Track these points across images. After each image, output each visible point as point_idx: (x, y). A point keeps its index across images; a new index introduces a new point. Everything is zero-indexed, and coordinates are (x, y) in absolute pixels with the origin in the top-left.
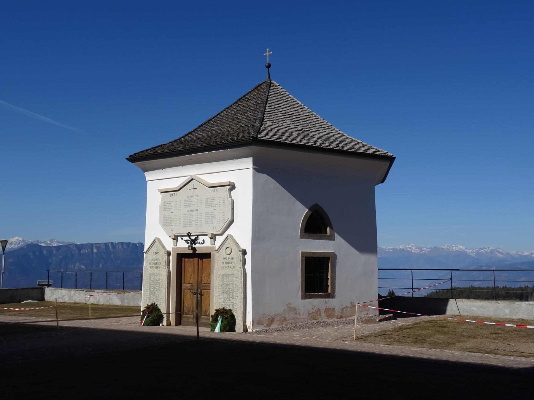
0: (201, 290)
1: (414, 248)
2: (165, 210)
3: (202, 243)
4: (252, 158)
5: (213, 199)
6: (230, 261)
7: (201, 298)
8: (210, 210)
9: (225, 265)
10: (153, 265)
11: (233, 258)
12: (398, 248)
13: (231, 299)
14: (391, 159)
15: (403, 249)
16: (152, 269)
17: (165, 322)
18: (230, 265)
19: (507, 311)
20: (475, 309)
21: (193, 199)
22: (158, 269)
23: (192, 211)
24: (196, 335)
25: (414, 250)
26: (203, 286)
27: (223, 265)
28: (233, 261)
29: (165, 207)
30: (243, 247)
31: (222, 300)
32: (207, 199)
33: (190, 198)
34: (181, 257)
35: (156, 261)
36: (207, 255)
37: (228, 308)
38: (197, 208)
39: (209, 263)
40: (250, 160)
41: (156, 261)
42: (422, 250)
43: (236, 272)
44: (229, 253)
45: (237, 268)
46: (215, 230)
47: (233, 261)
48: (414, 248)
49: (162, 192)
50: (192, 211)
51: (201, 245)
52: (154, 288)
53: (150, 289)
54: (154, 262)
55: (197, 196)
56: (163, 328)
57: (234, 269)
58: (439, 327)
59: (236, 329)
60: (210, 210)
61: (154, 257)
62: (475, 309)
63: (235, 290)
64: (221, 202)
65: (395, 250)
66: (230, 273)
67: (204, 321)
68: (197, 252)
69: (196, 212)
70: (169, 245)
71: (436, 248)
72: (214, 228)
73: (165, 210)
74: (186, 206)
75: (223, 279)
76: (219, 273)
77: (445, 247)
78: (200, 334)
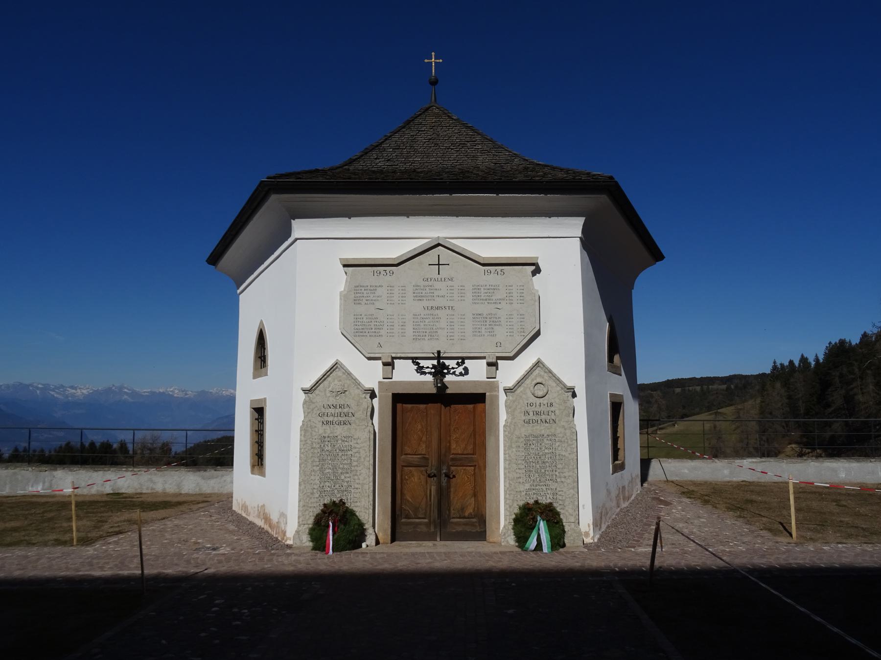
0: (448, 468)
1: (176, 391)
2: (357, 301)
3: (461, 374)
4: (579, 222)
5: (495, 288)
6: (543, 408)
7: (448, 482)
8: (485, 309)
9: (531, 416)
10: (330, 419)
11: (551, 405)
12: (157, 391)
13: (550, 483)
14: (658, 256)
15: (163, 393)
16: (327, 427)
17: (370, 540)
18: (543, 417)
19: (726, 472)
20: (686, 471)
21: (437, 285)
22: (346, 427)
23: (438, 308)
24: (648, 563)
25: (177, 394)
26: (453, 459)
27: (527, 418)
28: (552, 409)
29: (354, 297)
30: (368, 385)
31: (527, 486)
32: (476, 288)
33: (430, 283)
34: (401, 400)
35: (338, 410)
36: (477, 399)
37: (544, 500)
38: (450, 304)
39: (484, 411)
40: (579, 222)
41: (338, 410)
42: (186, 394)
43: (559, 430)
44: (540, 394)
45: (562, 423)
46: (499, 349)
47: (552, 409)
48: (176, 391)
49: (345, 266)
50: (438, 308)
51: (461, 378)
52: (334, 468)
53: (322, 470)
54: (332, 411)
55: (451, 279)
56: (378, 551)
57: (554, 425)
58: (755, 502)
59: (566, 541)
60: (485, 309)
61: (332, 401)
62: (686, 471)
63: (559, 466)
64: (515, 295)
65: (153, 394)
66: (546, 432)
67: (460, 529)
68: (448, 391)
69: (450, 312)
70: (370, 375)
71: (203, 392)
72: (498, 344)
73: (357, 301)
74: (419, 298)
75: (527, 444)
76: (517, 433)
77: (214, 391)
78: (657, 563)
